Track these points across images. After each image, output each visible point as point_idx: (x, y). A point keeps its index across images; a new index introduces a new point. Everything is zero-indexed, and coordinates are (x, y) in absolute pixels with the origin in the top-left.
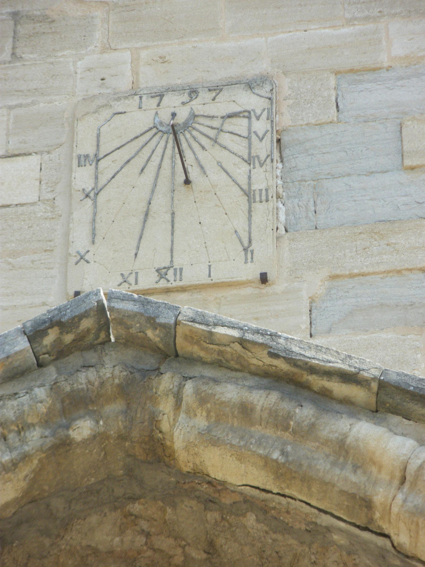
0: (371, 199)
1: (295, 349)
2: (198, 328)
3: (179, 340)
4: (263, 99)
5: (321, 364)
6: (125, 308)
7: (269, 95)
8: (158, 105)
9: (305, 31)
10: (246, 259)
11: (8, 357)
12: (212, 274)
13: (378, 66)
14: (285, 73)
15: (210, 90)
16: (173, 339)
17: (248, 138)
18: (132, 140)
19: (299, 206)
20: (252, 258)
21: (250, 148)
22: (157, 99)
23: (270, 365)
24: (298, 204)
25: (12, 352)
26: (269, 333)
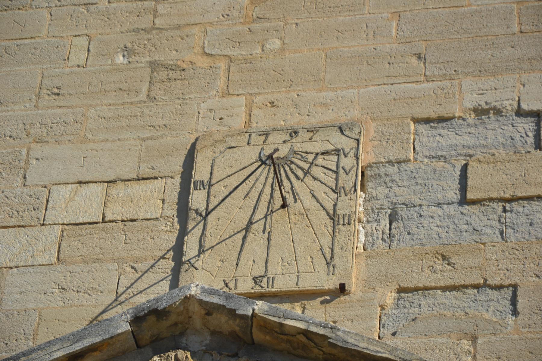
0: (437, 226)
1: (350, 340)
2: (271, 320)
3: (254, 330)
4: (352, 140)
5: (371, 353)
6: (212, 301)
7: (357, 137)
8: (264, 142)
9: (392, 84)
10: (329, 271)
11: (112, 338)
12: (299, 283)
13: (451, 115)
14: (373, 119)
15: (308, 131)
16: (249, 329)
17: (336, 172)
18: (241, 170)
19: (376, 230)
20: (334, 271)
21: (337, 180)
22: (263, 138)
23: (329, 354)
24: (376, 228)
25: (116, 333)
26: (330, 326)
